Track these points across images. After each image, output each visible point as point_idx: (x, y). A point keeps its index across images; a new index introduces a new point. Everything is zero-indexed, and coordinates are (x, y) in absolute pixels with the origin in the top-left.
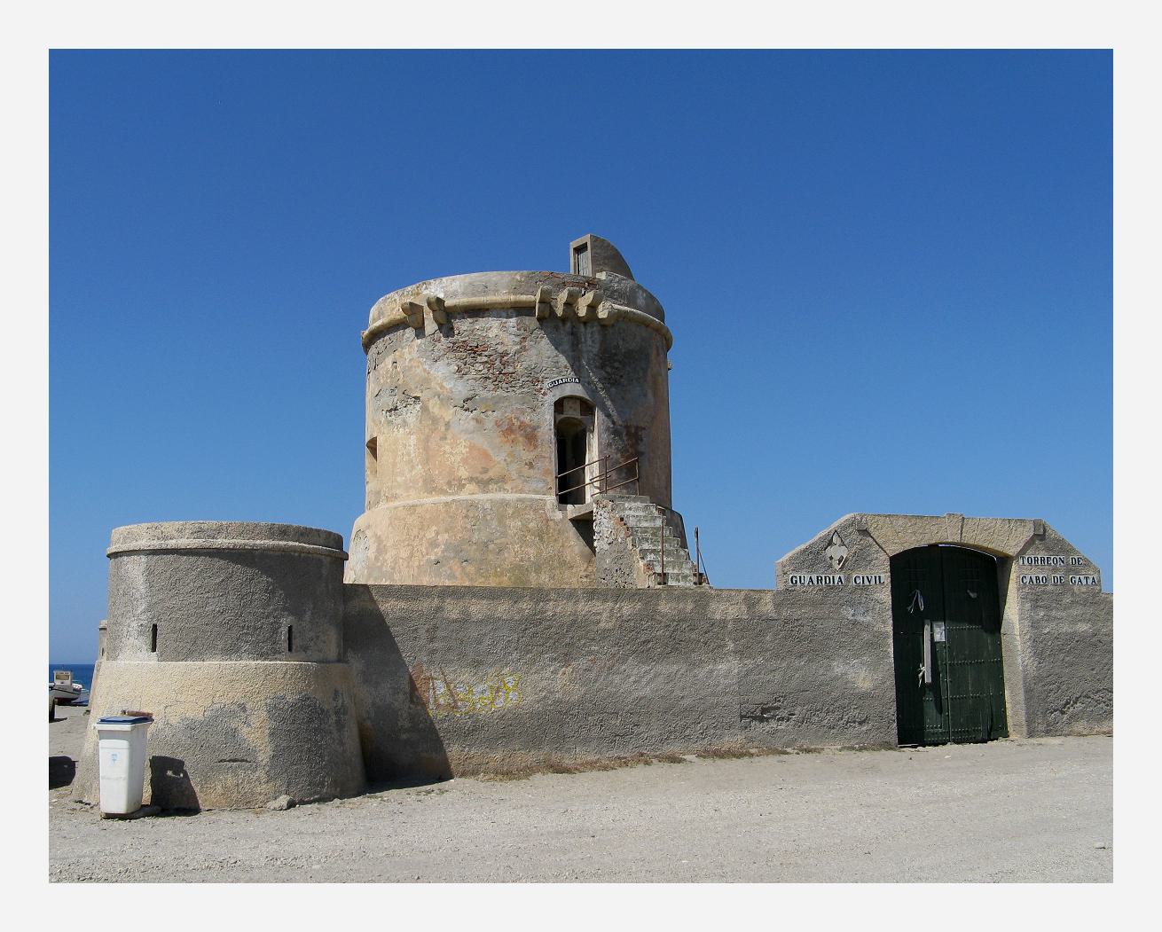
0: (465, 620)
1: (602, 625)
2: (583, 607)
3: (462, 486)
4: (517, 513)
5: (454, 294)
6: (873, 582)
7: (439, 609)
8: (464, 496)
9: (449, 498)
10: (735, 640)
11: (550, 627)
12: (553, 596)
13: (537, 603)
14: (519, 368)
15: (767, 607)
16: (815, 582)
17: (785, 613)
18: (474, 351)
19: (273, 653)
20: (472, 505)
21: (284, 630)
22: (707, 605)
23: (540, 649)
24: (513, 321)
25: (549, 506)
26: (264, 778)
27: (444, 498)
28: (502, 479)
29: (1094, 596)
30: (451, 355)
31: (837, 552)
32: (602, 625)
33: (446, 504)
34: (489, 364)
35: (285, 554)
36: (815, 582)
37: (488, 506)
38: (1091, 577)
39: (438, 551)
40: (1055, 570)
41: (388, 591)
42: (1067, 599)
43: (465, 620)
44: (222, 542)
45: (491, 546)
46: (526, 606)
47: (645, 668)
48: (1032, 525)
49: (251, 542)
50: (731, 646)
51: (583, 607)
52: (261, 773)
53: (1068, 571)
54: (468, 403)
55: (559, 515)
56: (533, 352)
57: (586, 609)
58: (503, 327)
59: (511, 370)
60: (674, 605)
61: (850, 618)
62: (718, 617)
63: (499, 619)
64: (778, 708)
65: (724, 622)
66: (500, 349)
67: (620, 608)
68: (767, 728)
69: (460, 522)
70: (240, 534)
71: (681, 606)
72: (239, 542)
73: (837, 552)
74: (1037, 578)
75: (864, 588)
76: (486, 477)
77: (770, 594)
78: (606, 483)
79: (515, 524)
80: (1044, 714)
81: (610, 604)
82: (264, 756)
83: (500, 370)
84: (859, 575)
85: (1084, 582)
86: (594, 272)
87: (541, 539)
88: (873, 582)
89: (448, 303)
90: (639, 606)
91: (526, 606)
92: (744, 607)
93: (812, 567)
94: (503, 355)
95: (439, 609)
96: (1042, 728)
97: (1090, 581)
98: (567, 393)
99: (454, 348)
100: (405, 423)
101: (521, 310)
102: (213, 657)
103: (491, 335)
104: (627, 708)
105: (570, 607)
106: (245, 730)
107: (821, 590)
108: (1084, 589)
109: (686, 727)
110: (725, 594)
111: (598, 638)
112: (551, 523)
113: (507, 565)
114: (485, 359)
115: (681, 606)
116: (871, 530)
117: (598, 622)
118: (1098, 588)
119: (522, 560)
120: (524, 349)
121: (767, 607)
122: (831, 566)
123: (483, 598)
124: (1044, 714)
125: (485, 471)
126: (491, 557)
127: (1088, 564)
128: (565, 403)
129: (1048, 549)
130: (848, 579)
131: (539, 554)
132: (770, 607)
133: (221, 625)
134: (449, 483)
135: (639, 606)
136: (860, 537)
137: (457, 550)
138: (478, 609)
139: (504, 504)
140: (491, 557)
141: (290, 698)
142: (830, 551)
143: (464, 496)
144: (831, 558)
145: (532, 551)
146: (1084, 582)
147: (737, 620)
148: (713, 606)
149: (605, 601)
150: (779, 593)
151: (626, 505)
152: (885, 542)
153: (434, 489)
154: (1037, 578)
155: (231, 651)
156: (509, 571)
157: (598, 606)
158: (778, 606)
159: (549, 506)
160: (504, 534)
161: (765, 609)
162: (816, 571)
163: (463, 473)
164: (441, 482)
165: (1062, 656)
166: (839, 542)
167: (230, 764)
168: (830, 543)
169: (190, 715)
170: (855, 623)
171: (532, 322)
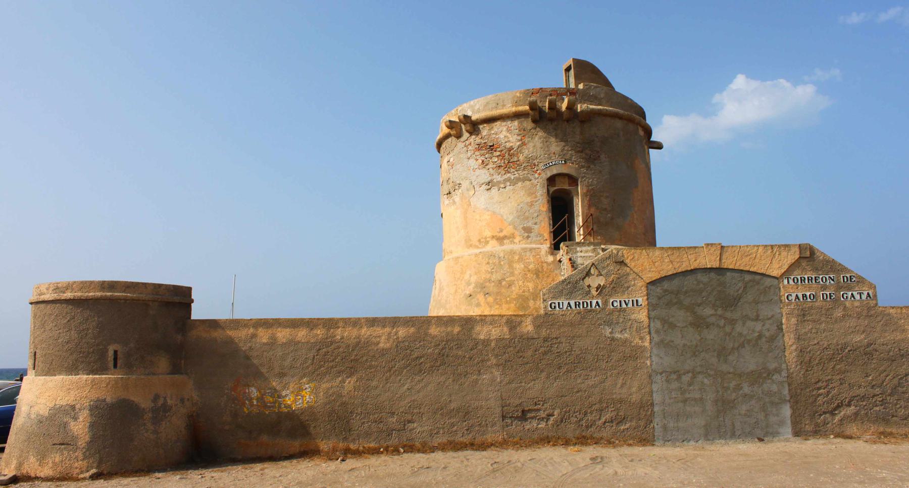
0: (273, 343)
1: (381, 345)
2: (365, 332)
3: (487, 243)
4: (521, 259)
5: (479, 111)
6: (630, 305)
7: (254, 336)
8: (488, 248)
9: (477, 251)
10: (496, 356)
11: (339, 347)
12: (341, 324)
13: (328, 330)
14: (521, 158)
15: (528, 327)
16: (573, 306)
17: (544, 333)
18: (492, 148)
19: (102, 370)
20: (492, 255)
21: (111, 353)
22: (472, 328)
23: (331, 364)
24: (516, 123)
25: (543, 253)
26: (81, 457)
27: (477, 251)
28: (511, 237)
29: (869, 309)
30: (477, 153)
31: (595, 281)
32: (381, 345)
33: (476, 255)
34: (502, 156)
35: (96, 300)
36: (573, 306)
37: (502, 255)
38: (866, 293)
39: (471, 287)
40: (824, 288)
41: (237, 324)
42: (839, 313)
43: (273, 343)
44: (69, 295)
45: (504, 283)
46: (320, 332)
47: (418, 378)
48: (797, 249)
49: (87, 294)
50: (494, 361)
51: (365, 332)
52: (79, 454)
53: (839, 288)
54: (490, 184)
55: (550, 259)
56: (531, 144)
57: (368, 333)
58: (509, 130)
59: (515, 159)
60: (443, 329)
61: (608, 334)
62: (482, 337)
63: (299, 342)
64: (539, 410)
65: (486, 342)
66: (508, 145)
67: (396, 333)
68: (527, 427)
69: (485, 268)
70: (80, 289)
71: (449, 329)
72: (79, 294)
73: (595, 281)
74: (804, 296)
75: (621, 310)
76: (502, 235)
77: (530, 317)
78: (588, 234)
79: (519, 267)
80: (812, 417)
81: (388, 329)
82: (83, 441)
83: (508, 160)
84: (616, 301)
85: (857, 297)
86: (577, 85)
87: (538, 276)
88: (630, 305)
89: (474, 118)
90: (412, 330)
91: (320, 332)
92: (506, 329)
93: (570, 295)
94: (511, 149)
95: (254, 336)
96: (809, 428)
97: (864, 297)
98: (555, 172)
99: (479, 147)
100: (454, 202)
101: (517, 116)
102: (60, 374)
103: (502, 136)
104: (401, 410)
105: (355, 332)
106: (72, 423)
107: (579, 313)
108: (857, 304)
109: (453, 425)
110: (488, 319)
111: (377, 356)
112: (545, 265)
113: (514, 296)
114: (498, 153)
115: (449, 329)
116: (627, 261)
117: (378, 343)
118: (874, 302)
119: (524, 292)
120: (524, 144)
121: (528, 327)
122: (589, 292)
123: (286, 327)
124: (812, 417)
125: (501, 231)
126: (503, 290)
127: (861, 281)
128: (557, 179)
129: (816, 270)
130: (606, 303)
131: (536, 287)
132: (530, 328)
133: (67, 351)
134: (479, 241)
135: (412, 330)
136: (618, 267)
137: (482, 287)
138: (282, 335)
139: (512, 252)
140: (503, 290)
141: (109, 400)
142: (588, 281)
143: (488, 248)
144: (589, 286)
145: (531, 285)
146: (857, 297)
147: (499, 340)
148: (478, 328)
149: (384, 326)
150: (538, 316)
151: (578, 249)
152: (642, 271)
153: (471, 246)
154: (804, 296)
155: (72, 369)
156: (515, 299)
157: (378, 330)
158: (538, 327)
159: (543, 253)
160: (512, 274)
161: (525, 330)
162: (575, 298)
163: (488, 233)
164: (475, 241)
165: (832, 364)
166: (597, 273)
167: (59, 447)
168: (588, 274)
169: (41, 412)
170: (613, 339)
171: (528, 124)
